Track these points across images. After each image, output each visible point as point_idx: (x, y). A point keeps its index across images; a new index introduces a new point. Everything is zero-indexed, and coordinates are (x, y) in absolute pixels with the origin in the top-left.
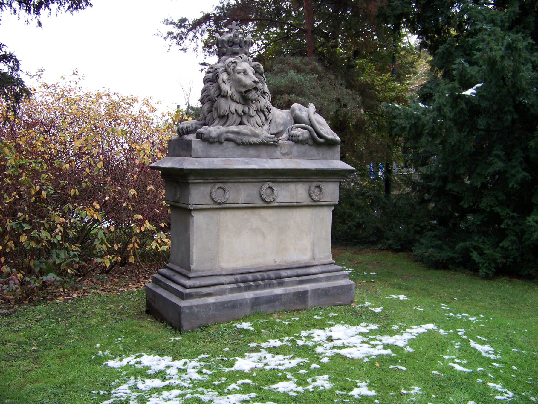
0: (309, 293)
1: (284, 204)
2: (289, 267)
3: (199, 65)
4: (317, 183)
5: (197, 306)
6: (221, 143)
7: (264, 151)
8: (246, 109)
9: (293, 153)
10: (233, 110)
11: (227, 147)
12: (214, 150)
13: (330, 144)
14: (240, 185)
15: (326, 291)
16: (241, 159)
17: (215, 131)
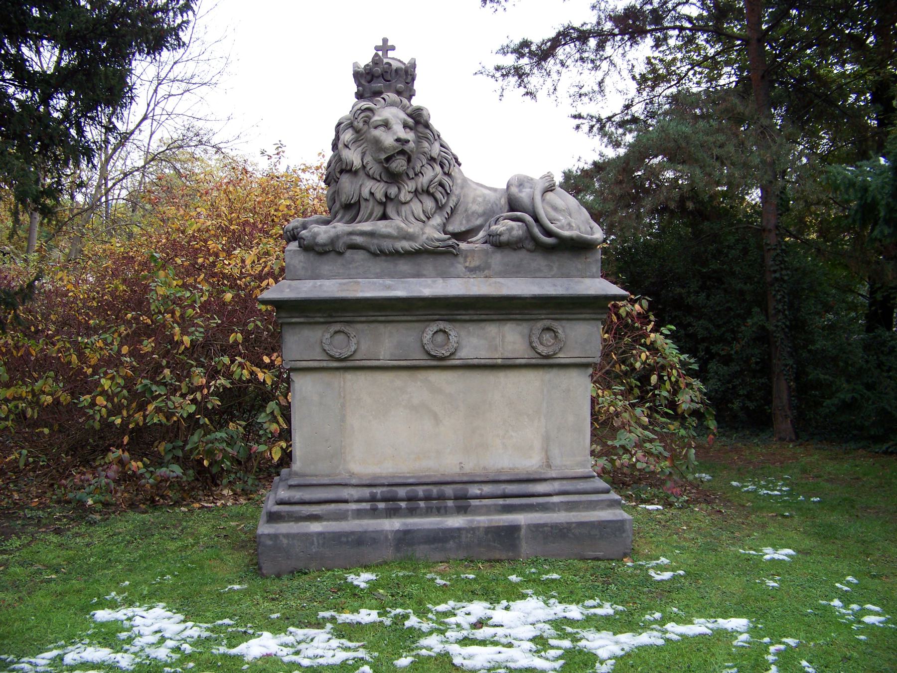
0: (523, 532)
1: (476, 362)
2: (491, 478)
3: (573, 120)
4: (547, 323)
5: (287, 536)
6: (340, 254)
7: (428, 265)
8: (393, 191)
9: (493, 266)
10: (365, 193)
11: (353, 261)
12: (327, 265)
13: (577, 247)
14: (381, 328)
15: (561, 530)
16: (381, 281)
17: (325, 232)
